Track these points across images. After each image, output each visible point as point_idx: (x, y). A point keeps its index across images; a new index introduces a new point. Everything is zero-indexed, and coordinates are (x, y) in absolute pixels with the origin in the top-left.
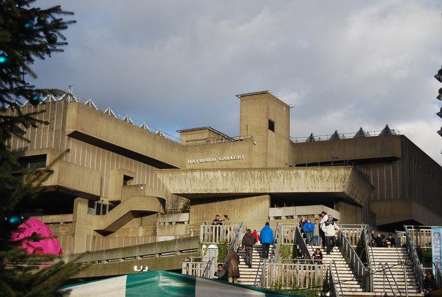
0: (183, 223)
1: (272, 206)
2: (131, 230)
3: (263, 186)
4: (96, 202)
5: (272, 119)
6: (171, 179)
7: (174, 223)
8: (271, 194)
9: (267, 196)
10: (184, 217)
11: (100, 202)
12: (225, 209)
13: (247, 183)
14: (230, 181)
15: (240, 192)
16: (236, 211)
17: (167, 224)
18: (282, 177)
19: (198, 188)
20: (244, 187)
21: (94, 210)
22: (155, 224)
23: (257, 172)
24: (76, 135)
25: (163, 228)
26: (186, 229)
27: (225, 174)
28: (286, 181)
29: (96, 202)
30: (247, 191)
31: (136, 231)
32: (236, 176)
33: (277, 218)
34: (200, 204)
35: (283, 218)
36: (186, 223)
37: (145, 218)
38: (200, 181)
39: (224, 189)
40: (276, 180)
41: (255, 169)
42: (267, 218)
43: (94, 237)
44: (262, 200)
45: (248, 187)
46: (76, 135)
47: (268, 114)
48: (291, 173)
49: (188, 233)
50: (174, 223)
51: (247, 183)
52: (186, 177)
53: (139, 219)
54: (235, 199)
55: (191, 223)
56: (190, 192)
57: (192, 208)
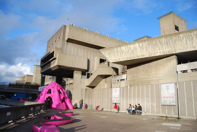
0: (124, 80)
1: (179, 63)
2: (102, 85)
3: (170, 49)
4: (87, 73)
5: (177, 25)
6: (109, 54)
7: (120, 81)
8: (177, 55)
9: (175, 56)
10: (124, 76)
11: (89, 72)
12: (146, 69)
13: (157, 48)
14: (145, 49)
15: (153, 55)
16: (153, 70)
17: (117, 81)
18: (185, 39)
19: (125, 57)
20: (156, 52)
21: (86, 77)
22: (111, 82)
23: (163, 39)
24: (70, 40)
25: (114, 83)
26: (126, 84)
27: (141, 45)
28: (188, 42)
29: (87, 73)
30: (158, 54)
31: (104, 86)
32: (149, 45)
33: (184, 71)
34: (130, 68)
35: (189, 71)
36: (125, 80)
37: (108, 78)
38: (126, 52)
39: (142, 55)
40: (179, 42)
41: (162, 37)
42: (129, 106)
43: (86, 89)
44: (170, 60)
45: (159, 51)
46: (70, 40)
47: (174, 22)
48: (192, 34)
49: (127, 86)
50: (120, 81)
51: (157, 48)
52: (117, 51)
53: (104, 80)
54: (158, 60)
55: (128, 79)
56: (121, 60)
57: (128, 71)
